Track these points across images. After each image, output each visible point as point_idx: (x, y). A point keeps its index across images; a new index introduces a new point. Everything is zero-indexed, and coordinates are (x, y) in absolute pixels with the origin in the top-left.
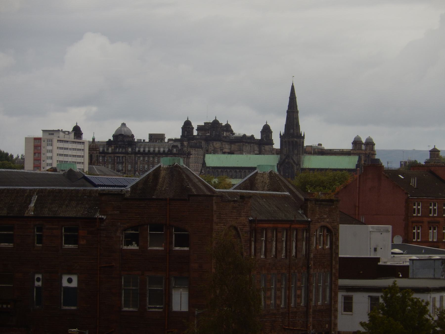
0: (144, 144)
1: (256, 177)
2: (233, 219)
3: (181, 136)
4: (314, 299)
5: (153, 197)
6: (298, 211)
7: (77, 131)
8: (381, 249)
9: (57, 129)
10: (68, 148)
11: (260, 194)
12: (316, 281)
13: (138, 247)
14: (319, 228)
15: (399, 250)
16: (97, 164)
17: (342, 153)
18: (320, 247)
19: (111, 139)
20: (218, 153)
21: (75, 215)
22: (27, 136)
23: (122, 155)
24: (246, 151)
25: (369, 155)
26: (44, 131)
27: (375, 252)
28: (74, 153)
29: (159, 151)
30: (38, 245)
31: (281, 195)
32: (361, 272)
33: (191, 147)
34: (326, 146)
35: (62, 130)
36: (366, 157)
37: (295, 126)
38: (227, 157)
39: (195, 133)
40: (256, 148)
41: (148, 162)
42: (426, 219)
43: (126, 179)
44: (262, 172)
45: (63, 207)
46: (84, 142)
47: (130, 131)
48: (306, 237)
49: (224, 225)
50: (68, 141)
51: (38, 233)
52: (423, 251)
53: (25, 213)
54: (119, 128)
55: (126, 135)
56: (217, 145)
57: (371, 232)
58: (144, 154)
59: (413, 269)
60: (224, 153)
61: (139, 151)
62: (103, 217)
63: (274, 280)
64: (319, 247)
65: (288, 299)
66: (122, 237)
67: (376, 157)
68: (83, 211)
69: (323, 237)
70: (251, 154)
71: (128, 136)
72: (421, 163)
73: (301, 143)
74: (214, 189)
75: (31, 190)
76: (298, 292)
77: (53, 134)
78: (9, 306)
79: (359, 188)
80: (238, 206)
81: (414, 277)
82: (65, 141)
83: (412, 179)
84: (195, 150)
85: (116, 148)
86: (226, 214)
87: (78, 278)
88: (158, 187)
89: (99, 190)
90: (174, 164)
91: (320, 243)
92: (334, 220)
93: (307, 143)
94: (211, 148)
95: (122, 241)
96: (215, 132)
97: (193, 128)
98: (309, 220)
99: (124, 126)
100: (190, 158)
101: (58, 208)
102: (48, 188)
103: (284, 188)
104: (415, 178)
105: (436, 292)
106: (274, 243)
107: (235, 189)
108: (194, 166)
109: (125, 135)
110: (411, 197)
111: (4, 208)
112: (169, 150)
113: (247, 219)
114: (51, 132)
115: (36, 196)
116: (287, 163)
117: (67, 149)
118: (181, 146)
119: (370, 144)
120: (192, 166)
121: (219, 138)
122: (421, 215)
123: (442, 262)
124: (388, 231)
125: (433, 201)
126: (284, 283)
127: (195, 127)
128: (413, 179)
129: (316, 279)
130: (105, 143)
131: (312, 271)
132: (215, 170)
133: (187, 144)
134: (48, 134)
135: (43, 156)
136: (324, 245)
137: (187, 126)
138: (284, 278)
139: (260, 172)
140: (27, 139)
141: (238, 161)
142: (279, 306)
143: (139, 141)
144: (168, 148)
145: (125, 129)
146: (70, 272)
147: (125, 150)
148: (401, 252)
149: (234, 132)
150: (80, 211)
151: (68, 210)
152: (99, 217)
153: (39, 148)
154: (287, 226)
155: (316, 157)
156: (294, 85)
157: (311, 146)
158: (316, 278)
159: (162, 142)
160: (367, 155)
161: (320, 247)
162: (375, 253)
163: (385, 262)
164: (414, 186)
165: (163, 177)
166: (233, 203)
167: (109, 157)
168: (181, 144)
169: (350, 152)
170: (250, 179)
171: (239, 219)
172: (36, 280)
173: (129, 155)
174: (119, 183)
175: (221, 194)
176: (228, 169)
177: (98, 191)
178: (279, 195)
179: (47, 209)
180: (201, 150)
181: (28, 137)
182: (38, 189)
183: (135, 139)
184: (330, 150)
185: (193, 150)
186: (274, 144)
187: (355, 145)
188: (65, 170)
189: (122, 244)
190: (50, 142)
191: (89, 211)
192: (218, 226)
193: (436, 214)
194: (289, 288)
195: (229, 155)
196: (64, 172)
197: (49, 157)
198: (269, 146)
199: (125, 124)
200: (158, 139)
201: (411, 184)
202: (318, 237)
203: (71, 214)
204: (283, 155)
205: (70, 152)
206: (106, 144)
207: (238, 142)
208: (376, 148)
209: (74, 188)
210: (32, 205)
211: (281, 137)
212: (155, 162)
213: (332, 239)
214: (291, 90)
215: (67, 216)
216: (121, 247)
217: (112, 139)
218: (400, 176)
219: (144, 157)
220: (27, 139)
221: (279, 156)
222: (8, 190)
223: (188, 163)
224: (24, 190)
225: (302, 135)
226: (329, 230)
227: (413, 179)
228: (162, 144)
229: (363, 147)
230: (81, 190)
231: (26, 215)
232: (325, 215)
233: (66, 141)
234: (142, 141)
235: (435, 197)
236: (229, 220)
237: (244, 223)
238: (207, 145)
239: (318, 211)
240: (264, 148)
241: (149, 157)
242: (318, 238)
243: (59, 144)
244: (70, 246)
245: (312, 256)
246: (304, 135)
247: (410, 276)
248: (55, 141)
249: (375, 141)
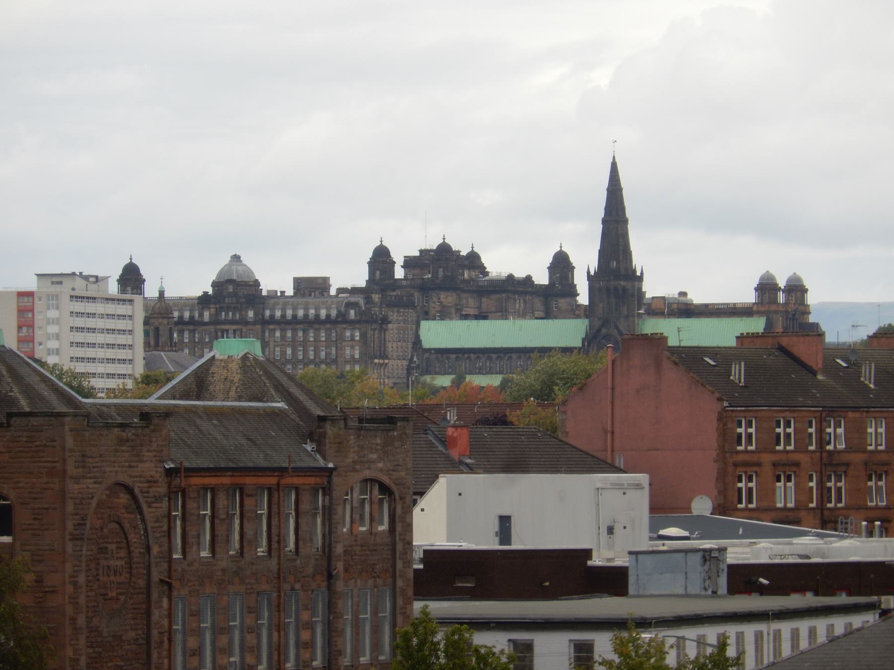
0: (282, 300)
2: (119, 467)
4: (349, 651)
6: (304, 445)
8: (625, 528)
9: (70, 272)
11: (205, 407)
12: (352, 609)
14: (359, 485)
15: (678, 529)
17: (734, 311)
18: (364, 529)
20: (451, 319)
23: (234, 327)
24: (515, 312)
25: (794, 315)
26: (40, 276)
27: (609, 536)
28: (111, 324)
29: (317, 316)
31: (264, 409)
32: (547, 584)
33: (390, 305)
34: (697, 298)
35: (81, 273)
36: (787, 319)
37: (621, 253)
38: (469, 326)
39: (399, 273)
40: (538, 303)
41: (294, 339)
42: (767, 458)
44: (226, 357)
47: (250, 272)
48: (324, 506)
49: (95, 483)
50: (95, 298)
52: (741, 532)
54: (226, 266)
55: (242, 281)
56: (448, 298)
57: (600, 490)
58: (284, 323)
59: (638, 575)
60: (466, 317)
61: (272, 316)
63: (238, 606)
64: (358, 528)
65: (276, 653)
67: (812, 319)
69: (371, 505)
70: (525, 319)
71: (245, 284)
73: (636, 292)
74: (80, 398)
77: (61, 283)
79: (613, 389)
81: (641, 593)
82: (88, 298)
83: (733, 366)
84: (398, 311)
85: (218, 311)
91: (362, 517)
92: (398, 465)
94: (435, 308)
96: (444, 271)
97: (394, 263)
98: (331, 465)
99: (237, 261)
100: (386, 330)
103: (274, 394)
104: (740, 365)
105: (664, 627)
106: (237, 522)
107: (160, 398)
108: (397, 347)
109: (239, 282)
110: (731, 408)
112: (340, 313)
113: (161, 467)
114: (57, 279)
116: (604, 337)
117: (93, 315)
118: (366, 304)
119: (796, 289)
120: (392, 347)
121: (450, 284)
122: (756, 448)
123: (704, 557)
124: (641, 487)
125: (783, 415)
126: (266, 614)
127: (399, 261)
128: (736, 365)
129: (352, 604)
130: (196, 301)
131: (340, 586)
132: (442, 357)
133: (379, 298)
134: (50, 283)
136: (373, 524)
138: (266, 603)
139: (221, 357)
141: (494, 335)
143: (272, 295)
144: (337, 308)
145: (240, 268)
147: (240, 315)
148: (685, 533)
149: (488, 270)
153: (30, 315)
154: (273, 481)
155: (669, 322)
157: (663, 298)
158: (352, 601)
159: (324, 295)
160: (790, 316)
161: (364, 529)
162: (610, 537)
163: (609, 560)
164: (740, 382)
168: (366, 298)
169: (751, 308)
170: (196, 373)
173: (250, 327)
176: (473, 353)
178: (258, 409)
180: (411, 312)
181: (5, 290)
183: (261, 290)
184: (706, 305)
185: (393, 312)
186: (578, 295)
187: (761, 293)
190: (53, 300)
192: (80, 486)
193: (741, 446)
194: (279, 627)
195: (475, 322)
197: (53, 334)
198: (568, 299)
199: (239, 257)
200: (314, 288)
201: (731, 378)
202: (355, 504)
204: (596, 319)
205: (100, 323)
206: (198, 304)
207: (495, 292)
208: (811, 299)
211: (589, 277)
212: (321, 341)
213: (395, 509)
214: (611, 172)
217: (210, 291)
218: (707, 359)
219: (283, 331)
221: (586, 321)
223: (383, 342)
225: (638, 274)
226: (384, 489)
227: (737, 366)
228: (324, 300)
229: (781, 298)
232: (373, 453)
233: (91, 298)
234: (279, 294)
235: (788, 407)
236: (108, 469)
237: (152, 476)
238: (426, 300)
239: (355, 443)
240: (555, 304)
241: (295, 331)
242: (356, 507)
243: (73, 305)
245: (339, 549)
246: (642, 273)
247: (631, 590)
249: (807, 284)
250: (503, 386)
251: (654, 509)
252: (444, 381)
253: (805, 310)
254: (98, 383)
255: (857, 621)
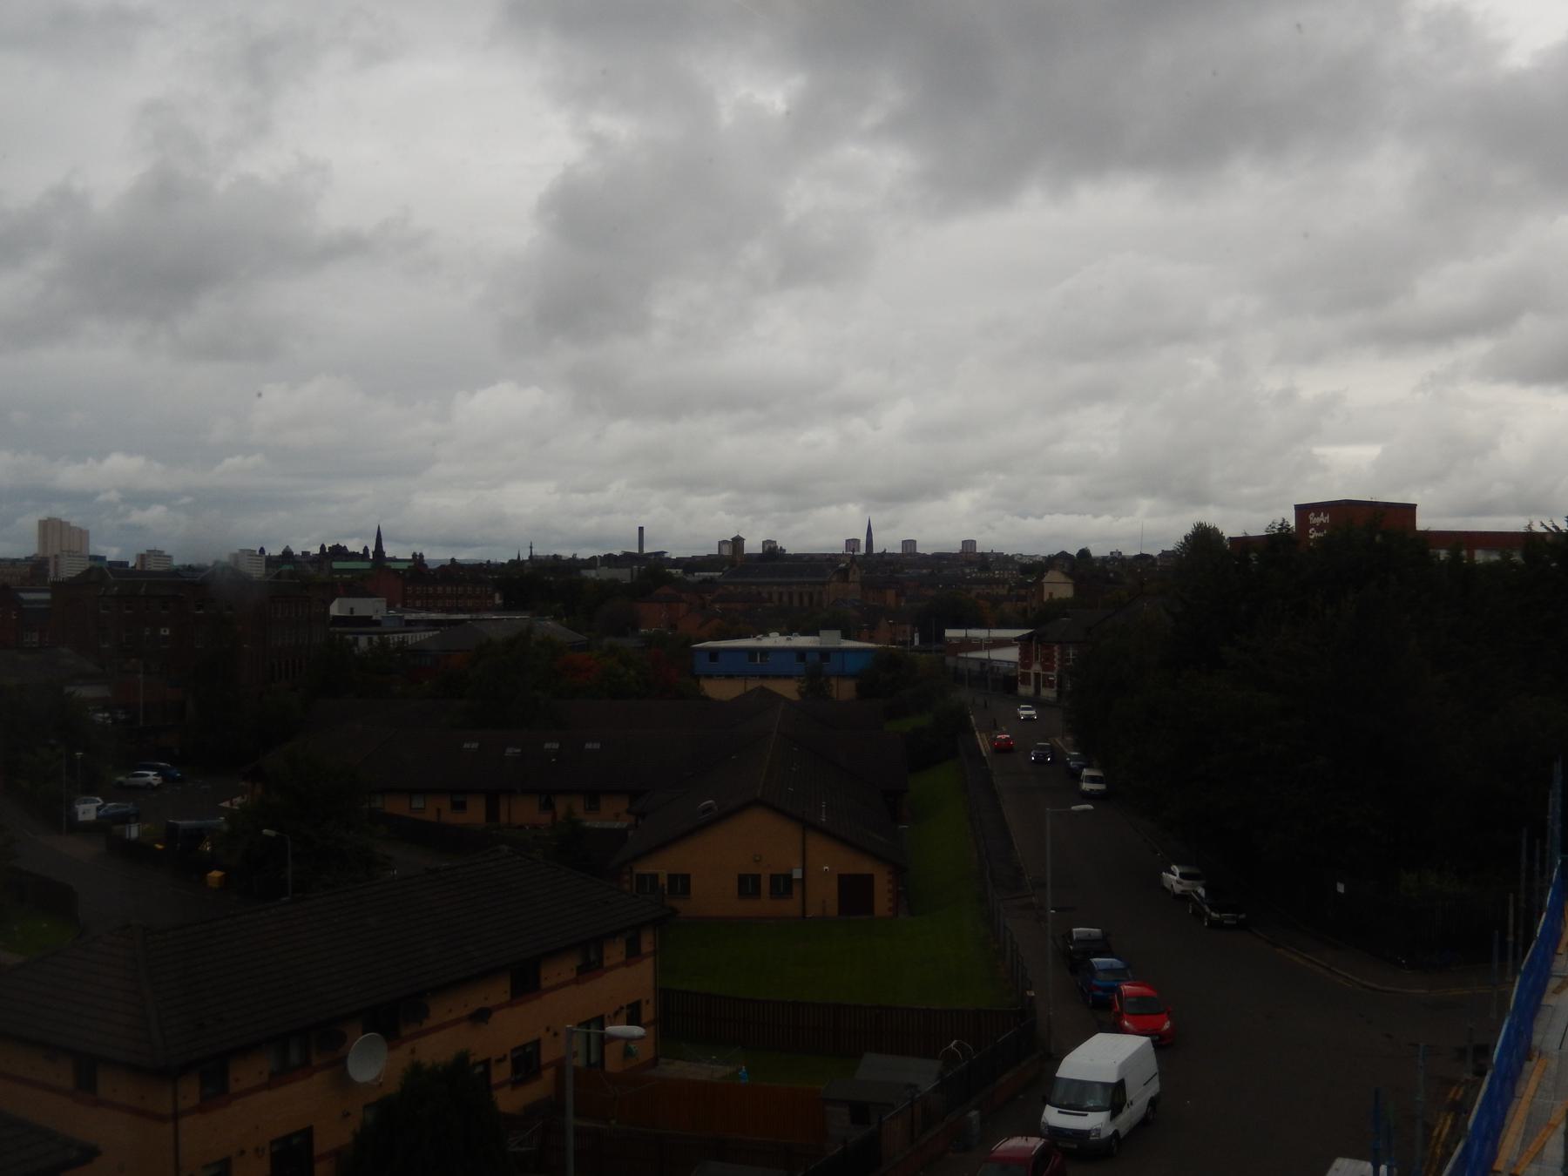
3: (738, 542)
7: (262, 551)
39: (327, 551)
72: (785, 550)
87: (1415, 527)
93: (387, 555)
119: (421, 556)
137: (323, 547)
156: (381, 539)
208: (425, 558)
250: (352, 578)
251: (388, 606)
252: (338, 576)
253: (423, 561)
254: (255, 576)
255: (435, 633)
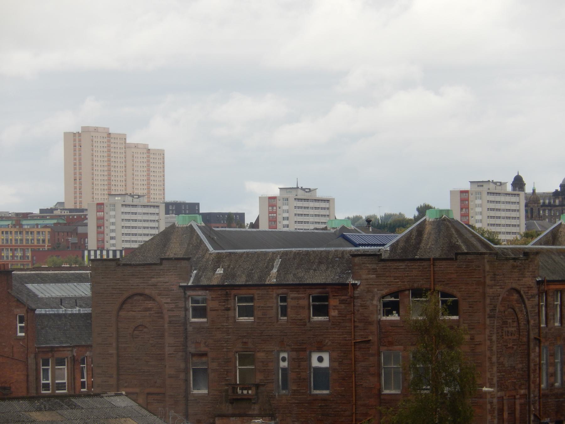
1: (559, 230)
5: (416, 257)
7: (518, 183)
9: (487, 180)
10: (500, 202)
13: (399, 317)
16: (539, 219)
19: (558, 190)
21: (324, 280)
22: (452, 189)
30: (282, 318)
35: (493, 181)
43: (376, 237)
45: (311, 272)
46: (519, 194)
49: (501, 288)
51: (317, 303)
53: (266, 281)
62: (356, 282)
66: (380, 305)
68: (333, 276)
74: (493, 245)
75: (273, 253)
76: (551, 370)
77: (482, 186)
78: (250, 392)
80: (520, 265)
82: (496, 193)
86: (503, 274)
88: (422, 245)
89: (352, 250)
90: (441, 217)
95: (380, 310)
101: (304, 274)
102: (293, 249)
111: (242, 275)
114: (480, 184)
115: (279, 260)
130: (552, 195)
134: (477, 186)
135: (471, 211)
140: (452, 192)
142: (552, 385)
146: (320, 349)
150: (331, 276)
151: (317, 275)
152: (351, 283)
153: (467, 202)
165: (428, 233)
166: (513, 261)
167: (556, 210)
171: (522, 280)
172: (286, 358)
174: (385, 241)
175: (502, 250)
177: (351, 252)
179: (291, 275)
181: (454, 190)
182: (282, 251)
188: (336, 228)
189: (380, 314)
191: (341, 276)
192: (494, 290)
196: (335, 230)
203: (319, 279)
206: (553, 196)
209: (324, 249)
210: (275, 270)
215: (315, 282)
216: (379, 317)
217: (559, 189)
220: (452, 192)
222: (248, 254)
224: (266, 254)
230: (332, 251)
231: (267, 283)
236: (507, 281)
237: (530, 285)
244: (320, 318)
248: (485, 194)
